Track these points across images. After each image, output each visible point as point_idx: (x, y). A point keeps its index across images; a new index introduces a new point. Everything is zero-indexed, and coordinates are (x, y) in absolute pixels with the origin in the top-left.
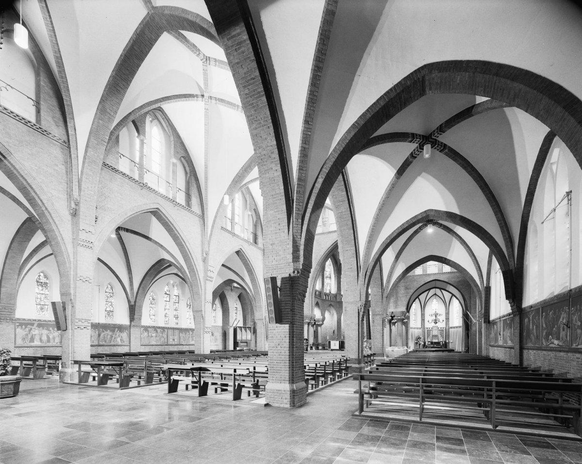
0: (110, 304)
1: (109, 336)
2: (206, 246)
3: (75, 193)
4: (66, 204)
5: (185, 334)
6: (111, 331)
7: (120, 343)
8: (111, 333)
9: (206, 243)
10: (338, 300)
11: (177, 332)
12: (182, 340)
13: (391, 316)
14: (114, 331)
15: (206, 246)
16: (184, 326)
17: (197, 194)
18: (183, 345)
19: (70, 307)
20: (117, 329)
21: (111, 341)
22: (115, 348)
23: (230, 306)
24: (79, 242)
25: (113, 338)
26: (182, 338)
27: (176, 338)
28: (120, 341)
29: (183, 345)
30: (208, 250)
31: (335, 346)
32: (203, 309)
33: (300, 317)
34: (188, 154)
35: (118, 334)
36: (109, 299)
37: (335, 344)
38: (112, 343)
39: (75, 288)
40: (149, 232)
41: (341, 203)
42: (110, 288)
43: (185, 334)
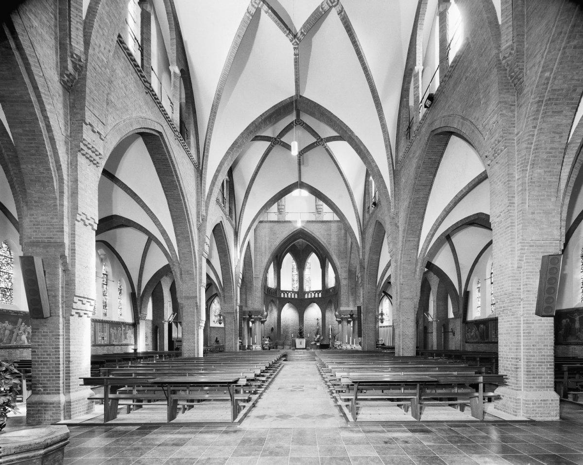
0: (6, 276)
1: (7, 332)
2: (203, 208)
3: (78, 46)
4: (55, 58)
5: (117, 330)
6: (11, 322)
7: (26, 343)
8: (10, 327)
9: (203, 203)
10: (278, 296)
11: (107, 326)
12: (113, 338)
13: (249, 315)
14: (15, 323)
15: (203, 208)
16: (115, 318)
17: (194, 132)
18: (114, 345)
19: (60, 270)
20: (20, 320)
21: (11, 340)
22: (18, 351)
23: (164, 294)
24: (82, 146)
25: (15, 334)
26: (113, 335)
27: (106, 334)
28: (26, 341)
29: (114, 345)
30: (205, 214)
31: (301, 344)
32: (198, 296)
33: (512, 321)
34: (188, 70)
35: (22, 328)
36: (4, 268)
37: (301, 344)
38: (14, 344)
39: (73, 235)
40: (115, 172)
41: (423, 187)
42: (6, 249)
43: (117, 330)
